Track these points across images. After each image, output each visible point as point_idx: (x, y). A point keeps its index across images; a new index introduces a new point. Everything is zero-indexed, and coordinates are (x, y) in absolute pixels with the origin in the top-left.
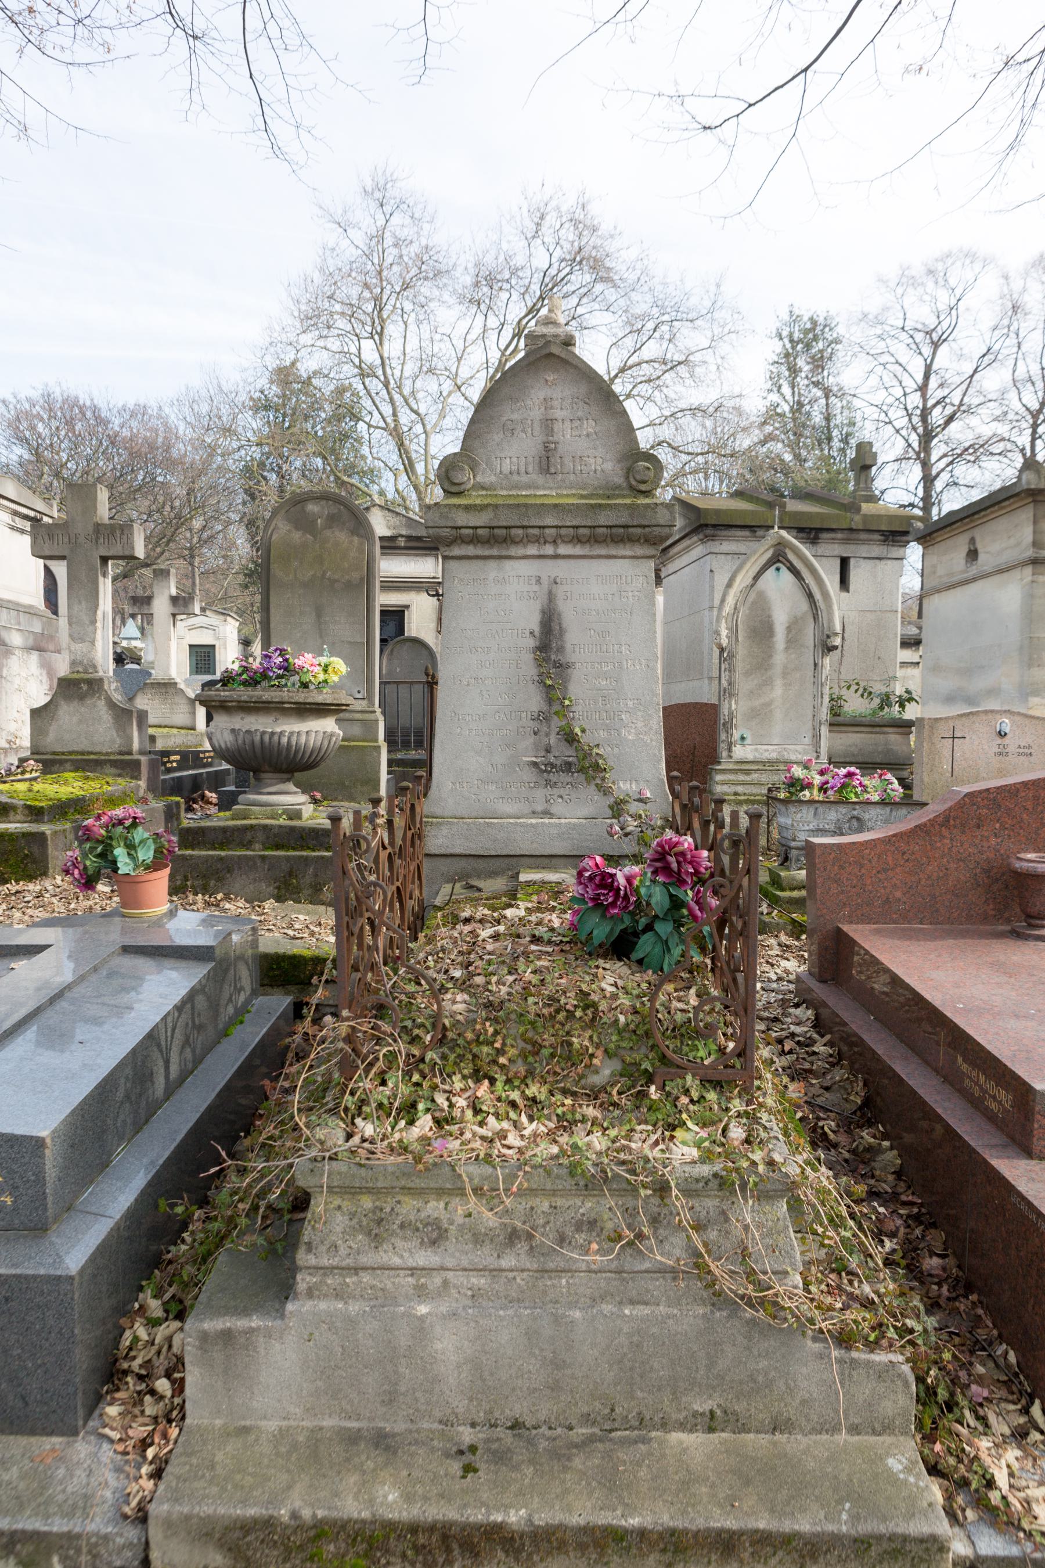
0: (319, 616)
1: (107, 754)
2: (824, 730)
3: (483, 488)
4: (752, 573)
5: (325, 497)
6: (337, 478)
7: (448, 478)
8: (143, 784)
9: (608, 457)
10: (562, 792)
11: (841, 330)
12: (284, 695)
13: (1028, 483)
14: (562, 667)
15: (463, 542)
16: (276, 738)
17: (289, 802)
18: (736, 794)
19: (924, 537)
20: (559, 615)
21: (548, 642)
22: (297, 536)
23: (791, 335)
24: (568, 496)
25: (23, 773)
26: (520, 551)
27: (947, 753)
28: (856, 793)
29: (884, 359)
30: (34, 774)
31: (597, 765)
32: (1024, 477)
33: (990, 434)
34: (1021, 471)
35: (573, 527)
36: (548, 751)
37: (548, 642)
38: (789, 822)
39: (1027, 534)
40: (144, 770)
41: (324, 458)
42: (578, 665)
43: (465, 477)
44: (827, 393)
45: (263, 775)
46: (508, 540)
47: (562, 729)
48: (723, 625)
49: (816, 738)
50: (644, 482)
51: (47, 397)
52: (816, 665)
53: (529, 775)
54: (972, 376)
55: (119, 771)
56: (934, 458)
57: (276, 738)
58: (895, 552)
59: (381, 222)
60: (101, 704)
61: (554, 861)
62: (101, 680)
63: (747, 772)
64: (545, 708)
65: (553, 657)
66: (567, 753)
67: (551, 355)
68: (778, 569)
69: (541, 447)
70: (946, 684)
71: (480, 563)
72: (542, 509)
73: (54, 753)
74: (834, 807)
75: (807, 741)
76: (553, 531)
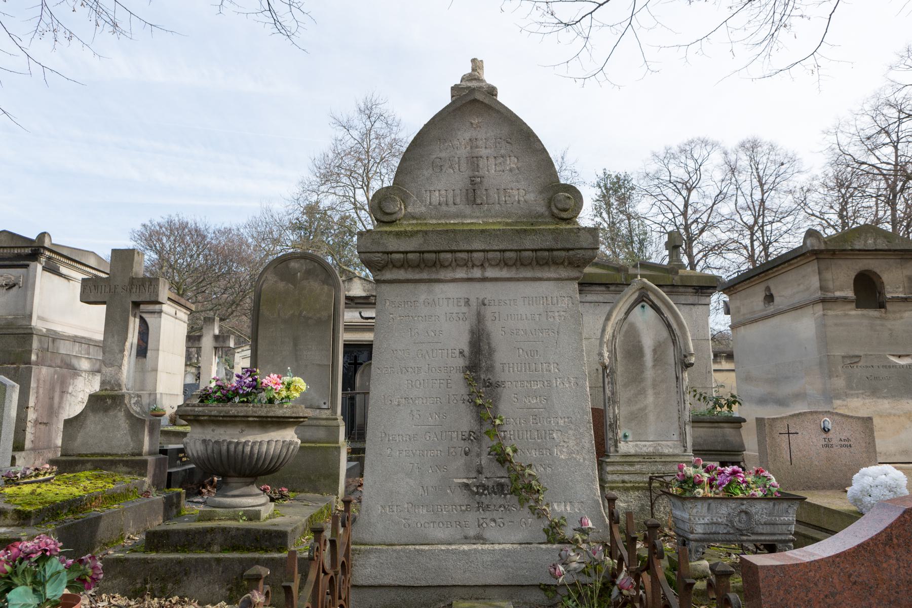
0: (295, 345)
1: (122, 455)
2: (688, 429)
3: (414, 218)
4: (624, 310)
5: (304, 257)
6: (340, 267)
7: (381, 209)
8: (148, 480)
9: (530, 189)
10: (495, 515)
11: (634, 182)
12: (249, 409)
13: (812, 246)
14: (492, 386)
15: (394, 266)
16: (240, 447)
17: (255, 504)
18: (623, 482)
19: (729, 288)
20: (488, 335)
21: (478, 361)
22: (281, 285)
23: (605, 185)
24: (493, 223)
25: (36, 476)
26: (449, 274)
27: (785, 445)
28: (741, 489)
29: (662, 197)
30: (47, 476)
31: (530, 486)
32: (808, 242)
33: (727, 238)
34: (805, 238)
35: (500, 251)
36: (480, 472)
37: (478, 361)
38: (686, 516)
39: (815, 282)
40: (151, 469)
41: (332, 256)
42: (508, 384)
43: (397, 207)
44: (629, 217)
45: (229, 480)
46: (437, 264)
47: (493, 449)
48: (605, 349)
49: (683, 435)
50: (565, 210)
51: (170, 222)
52: (677, 378)
53: (461, 498)
54: (712, 207)
55: (129, 470)
56: (695, 251)
57: (240, 447)
58: (703, 300)
59: (369, 125)
60: (121, 415)
61: (489, 591)
62: (123, 396)
63: (631, 464)
64: (476, 428)
65: (483, 377)
66: (499, 474)
67: (475, 101)
68: (643, 307)
69: (468, 181)
70: (759, 390)
71: (411, 286)
72: (470, 234)
73: (79, 455)
74: (724, 503)
75: (675, 437)
76: (481, 255)
